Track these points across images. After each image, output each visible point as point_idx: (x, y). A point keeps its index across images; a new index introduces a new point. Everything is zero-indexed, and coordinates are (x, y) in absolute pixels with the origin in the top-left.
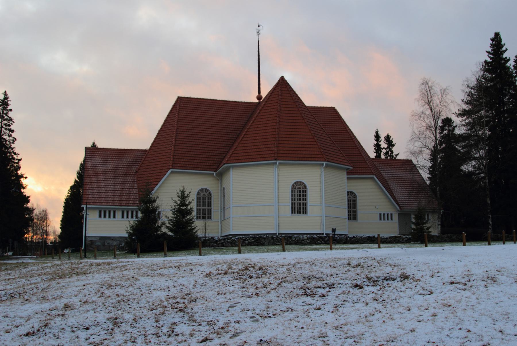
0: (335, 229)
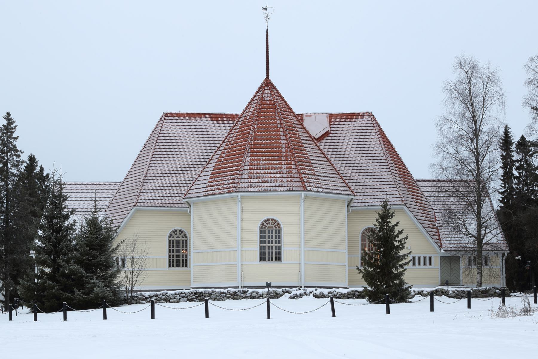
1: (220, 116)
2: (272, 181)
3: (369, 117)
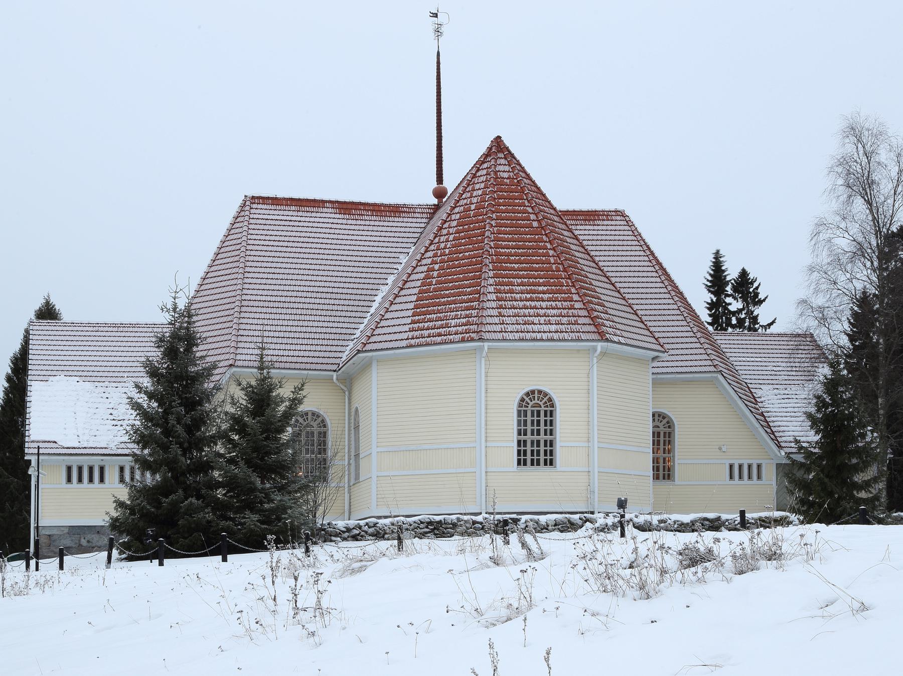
0: (626, 501)
1: (354, 207)
2: (542, 322)
3: (622, 218)
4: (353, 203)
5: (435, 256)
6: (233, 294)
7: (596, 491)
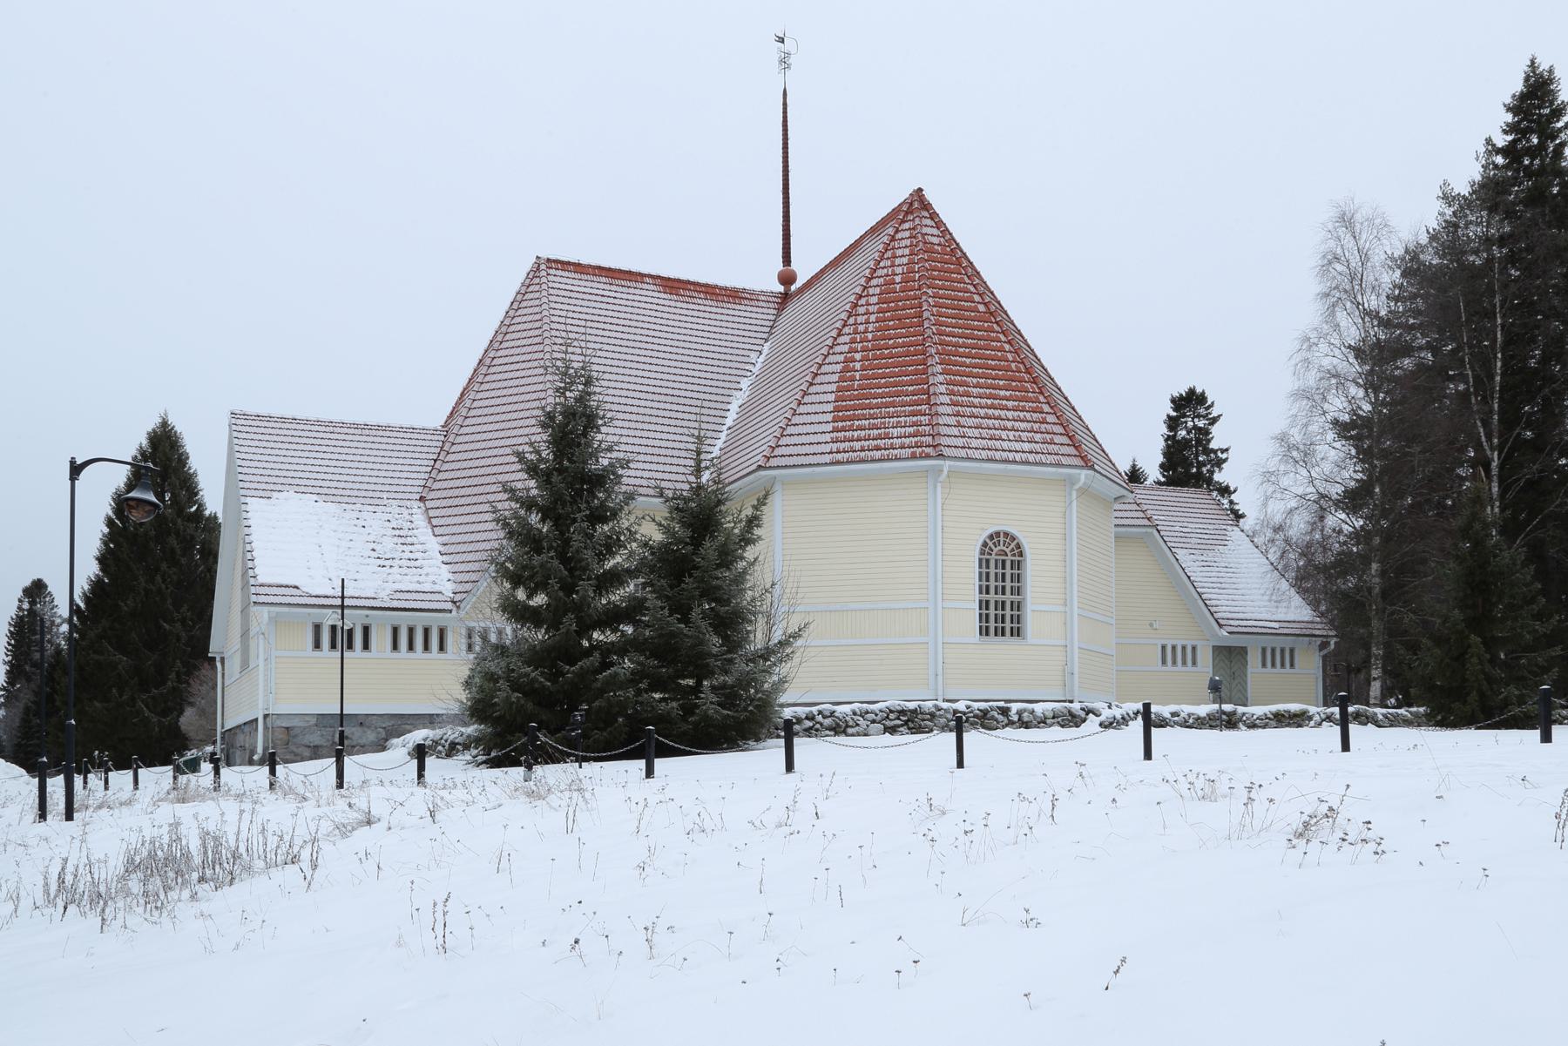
4: (679, 281)
5: (853, 341)
6: (541, 387)
7: (1076, 671)
